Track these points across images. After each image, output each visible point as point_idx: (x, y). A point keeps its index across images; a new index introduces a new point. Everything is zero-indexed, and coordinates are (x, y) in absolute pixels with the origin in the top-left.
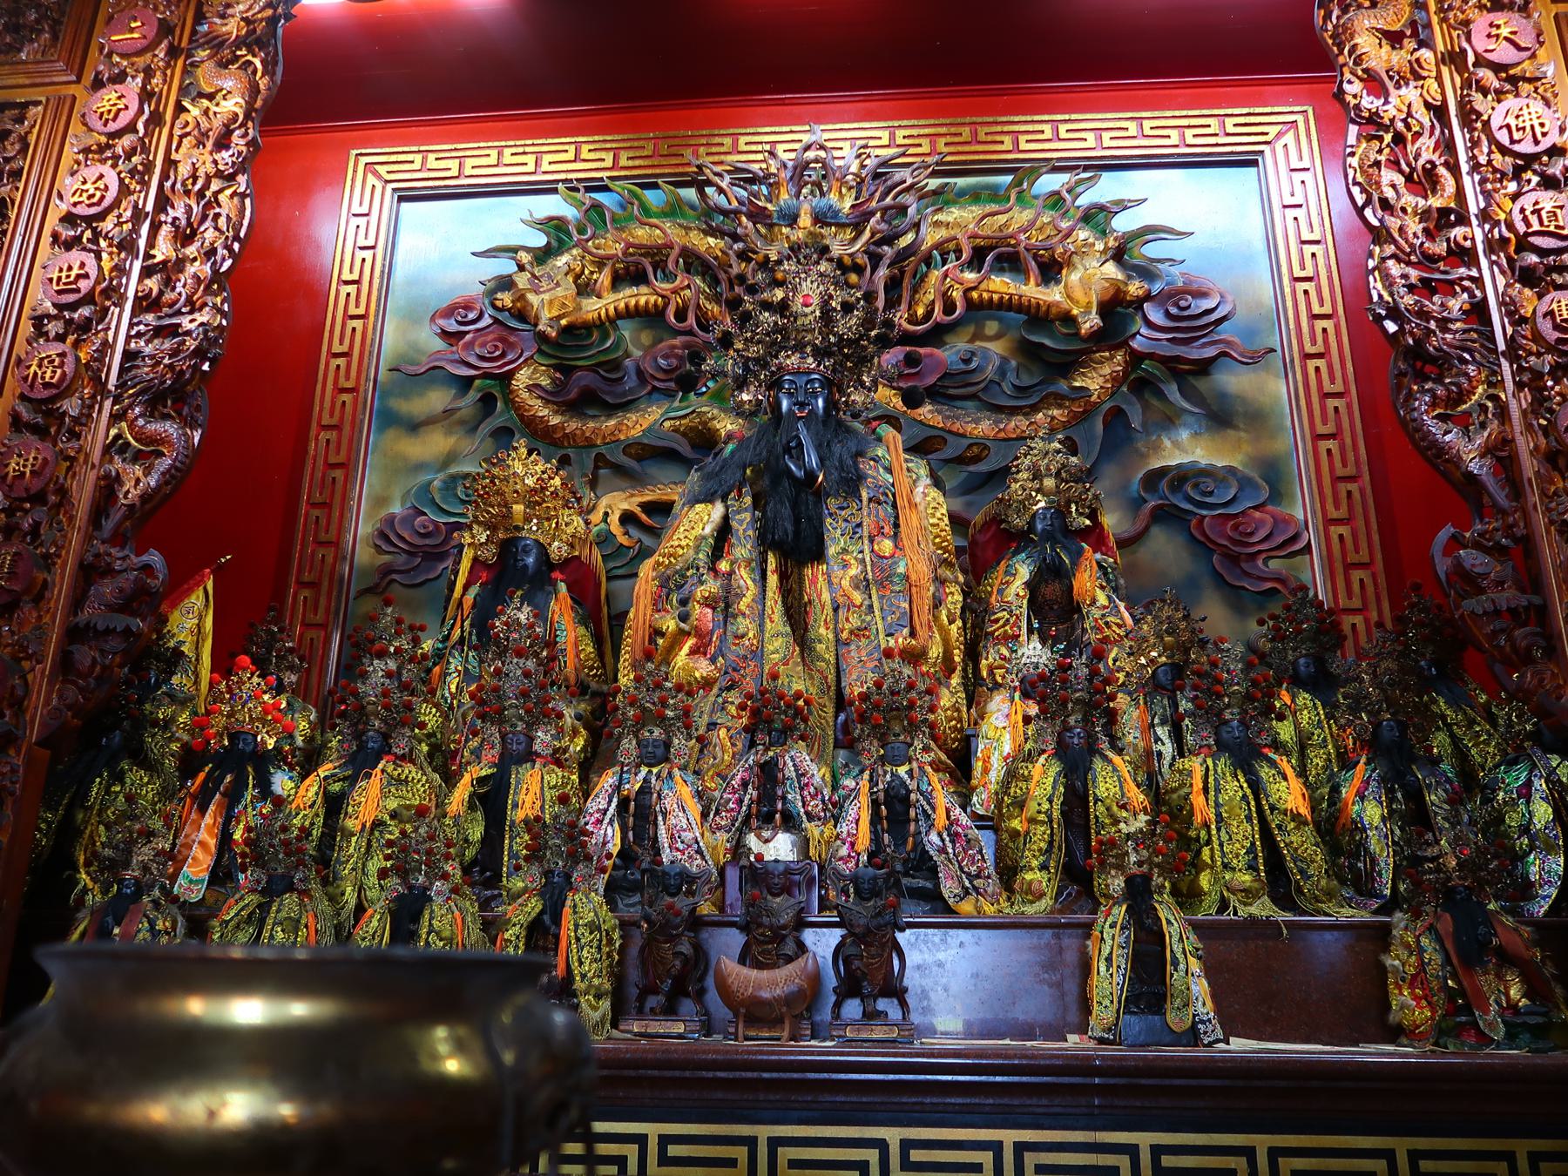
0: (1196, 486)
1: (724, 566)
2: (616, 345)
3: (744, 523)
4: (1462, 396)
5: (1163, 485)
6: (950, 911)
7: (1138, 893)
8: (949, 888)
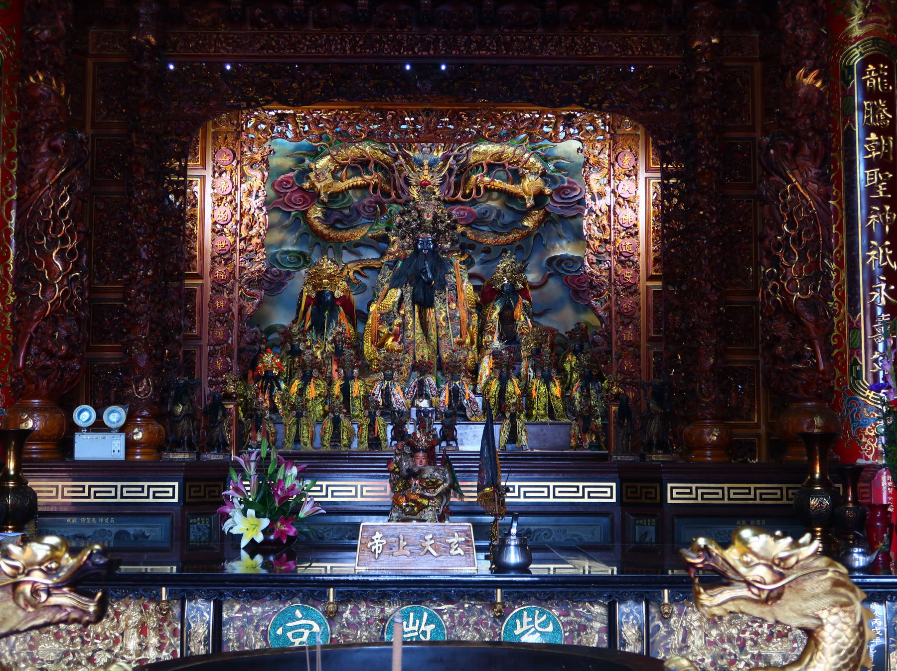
0: (566, 264)
1: (402, 312)
2: (349, 201)
3: (408, 297)
4: (601, 294)
5: (554, 263)
6: (469, 420)
8: (468, 414)
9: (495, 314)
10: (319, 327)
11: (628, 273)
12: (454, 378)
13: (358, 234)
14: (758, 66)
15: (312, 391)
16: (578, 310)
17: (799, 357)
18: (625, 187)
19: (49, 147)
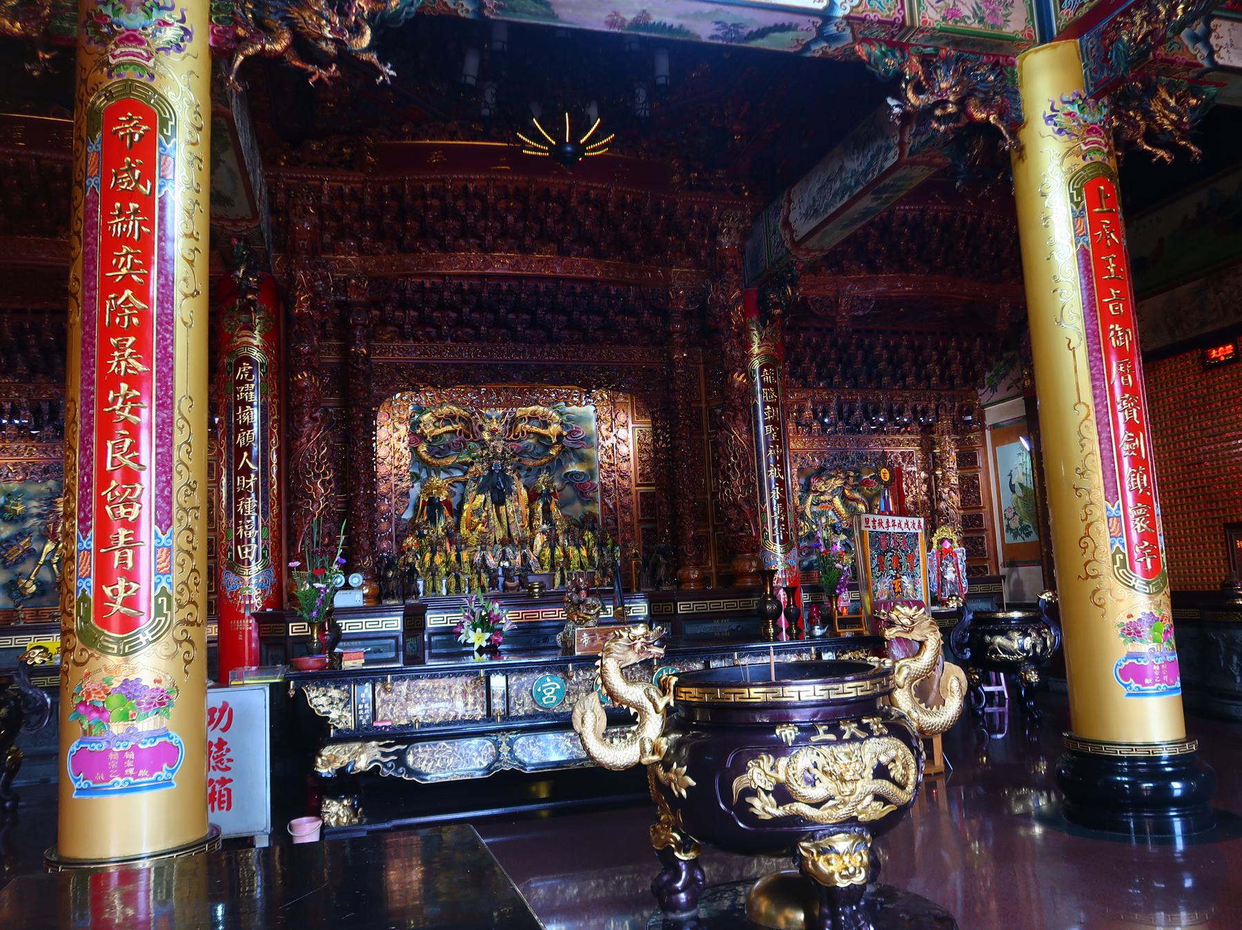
7: (562, 570)
9: (540, 509)
10: (432, 519)
11: (626, 483)
12: (523, 548)
13: (450, 461)
14: (701, 367)
15: (438, 559)
16: (584, 503)
17: (742, 529)
18: (622, 433)
19: (311, 417)
